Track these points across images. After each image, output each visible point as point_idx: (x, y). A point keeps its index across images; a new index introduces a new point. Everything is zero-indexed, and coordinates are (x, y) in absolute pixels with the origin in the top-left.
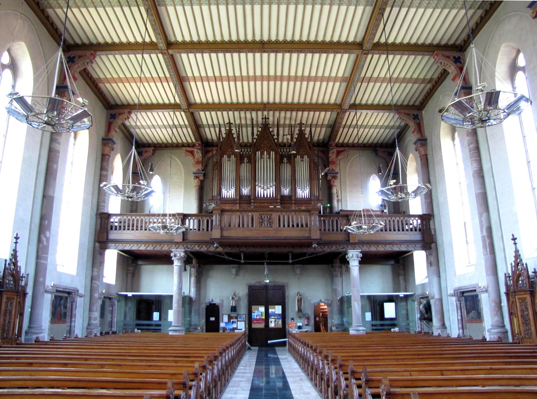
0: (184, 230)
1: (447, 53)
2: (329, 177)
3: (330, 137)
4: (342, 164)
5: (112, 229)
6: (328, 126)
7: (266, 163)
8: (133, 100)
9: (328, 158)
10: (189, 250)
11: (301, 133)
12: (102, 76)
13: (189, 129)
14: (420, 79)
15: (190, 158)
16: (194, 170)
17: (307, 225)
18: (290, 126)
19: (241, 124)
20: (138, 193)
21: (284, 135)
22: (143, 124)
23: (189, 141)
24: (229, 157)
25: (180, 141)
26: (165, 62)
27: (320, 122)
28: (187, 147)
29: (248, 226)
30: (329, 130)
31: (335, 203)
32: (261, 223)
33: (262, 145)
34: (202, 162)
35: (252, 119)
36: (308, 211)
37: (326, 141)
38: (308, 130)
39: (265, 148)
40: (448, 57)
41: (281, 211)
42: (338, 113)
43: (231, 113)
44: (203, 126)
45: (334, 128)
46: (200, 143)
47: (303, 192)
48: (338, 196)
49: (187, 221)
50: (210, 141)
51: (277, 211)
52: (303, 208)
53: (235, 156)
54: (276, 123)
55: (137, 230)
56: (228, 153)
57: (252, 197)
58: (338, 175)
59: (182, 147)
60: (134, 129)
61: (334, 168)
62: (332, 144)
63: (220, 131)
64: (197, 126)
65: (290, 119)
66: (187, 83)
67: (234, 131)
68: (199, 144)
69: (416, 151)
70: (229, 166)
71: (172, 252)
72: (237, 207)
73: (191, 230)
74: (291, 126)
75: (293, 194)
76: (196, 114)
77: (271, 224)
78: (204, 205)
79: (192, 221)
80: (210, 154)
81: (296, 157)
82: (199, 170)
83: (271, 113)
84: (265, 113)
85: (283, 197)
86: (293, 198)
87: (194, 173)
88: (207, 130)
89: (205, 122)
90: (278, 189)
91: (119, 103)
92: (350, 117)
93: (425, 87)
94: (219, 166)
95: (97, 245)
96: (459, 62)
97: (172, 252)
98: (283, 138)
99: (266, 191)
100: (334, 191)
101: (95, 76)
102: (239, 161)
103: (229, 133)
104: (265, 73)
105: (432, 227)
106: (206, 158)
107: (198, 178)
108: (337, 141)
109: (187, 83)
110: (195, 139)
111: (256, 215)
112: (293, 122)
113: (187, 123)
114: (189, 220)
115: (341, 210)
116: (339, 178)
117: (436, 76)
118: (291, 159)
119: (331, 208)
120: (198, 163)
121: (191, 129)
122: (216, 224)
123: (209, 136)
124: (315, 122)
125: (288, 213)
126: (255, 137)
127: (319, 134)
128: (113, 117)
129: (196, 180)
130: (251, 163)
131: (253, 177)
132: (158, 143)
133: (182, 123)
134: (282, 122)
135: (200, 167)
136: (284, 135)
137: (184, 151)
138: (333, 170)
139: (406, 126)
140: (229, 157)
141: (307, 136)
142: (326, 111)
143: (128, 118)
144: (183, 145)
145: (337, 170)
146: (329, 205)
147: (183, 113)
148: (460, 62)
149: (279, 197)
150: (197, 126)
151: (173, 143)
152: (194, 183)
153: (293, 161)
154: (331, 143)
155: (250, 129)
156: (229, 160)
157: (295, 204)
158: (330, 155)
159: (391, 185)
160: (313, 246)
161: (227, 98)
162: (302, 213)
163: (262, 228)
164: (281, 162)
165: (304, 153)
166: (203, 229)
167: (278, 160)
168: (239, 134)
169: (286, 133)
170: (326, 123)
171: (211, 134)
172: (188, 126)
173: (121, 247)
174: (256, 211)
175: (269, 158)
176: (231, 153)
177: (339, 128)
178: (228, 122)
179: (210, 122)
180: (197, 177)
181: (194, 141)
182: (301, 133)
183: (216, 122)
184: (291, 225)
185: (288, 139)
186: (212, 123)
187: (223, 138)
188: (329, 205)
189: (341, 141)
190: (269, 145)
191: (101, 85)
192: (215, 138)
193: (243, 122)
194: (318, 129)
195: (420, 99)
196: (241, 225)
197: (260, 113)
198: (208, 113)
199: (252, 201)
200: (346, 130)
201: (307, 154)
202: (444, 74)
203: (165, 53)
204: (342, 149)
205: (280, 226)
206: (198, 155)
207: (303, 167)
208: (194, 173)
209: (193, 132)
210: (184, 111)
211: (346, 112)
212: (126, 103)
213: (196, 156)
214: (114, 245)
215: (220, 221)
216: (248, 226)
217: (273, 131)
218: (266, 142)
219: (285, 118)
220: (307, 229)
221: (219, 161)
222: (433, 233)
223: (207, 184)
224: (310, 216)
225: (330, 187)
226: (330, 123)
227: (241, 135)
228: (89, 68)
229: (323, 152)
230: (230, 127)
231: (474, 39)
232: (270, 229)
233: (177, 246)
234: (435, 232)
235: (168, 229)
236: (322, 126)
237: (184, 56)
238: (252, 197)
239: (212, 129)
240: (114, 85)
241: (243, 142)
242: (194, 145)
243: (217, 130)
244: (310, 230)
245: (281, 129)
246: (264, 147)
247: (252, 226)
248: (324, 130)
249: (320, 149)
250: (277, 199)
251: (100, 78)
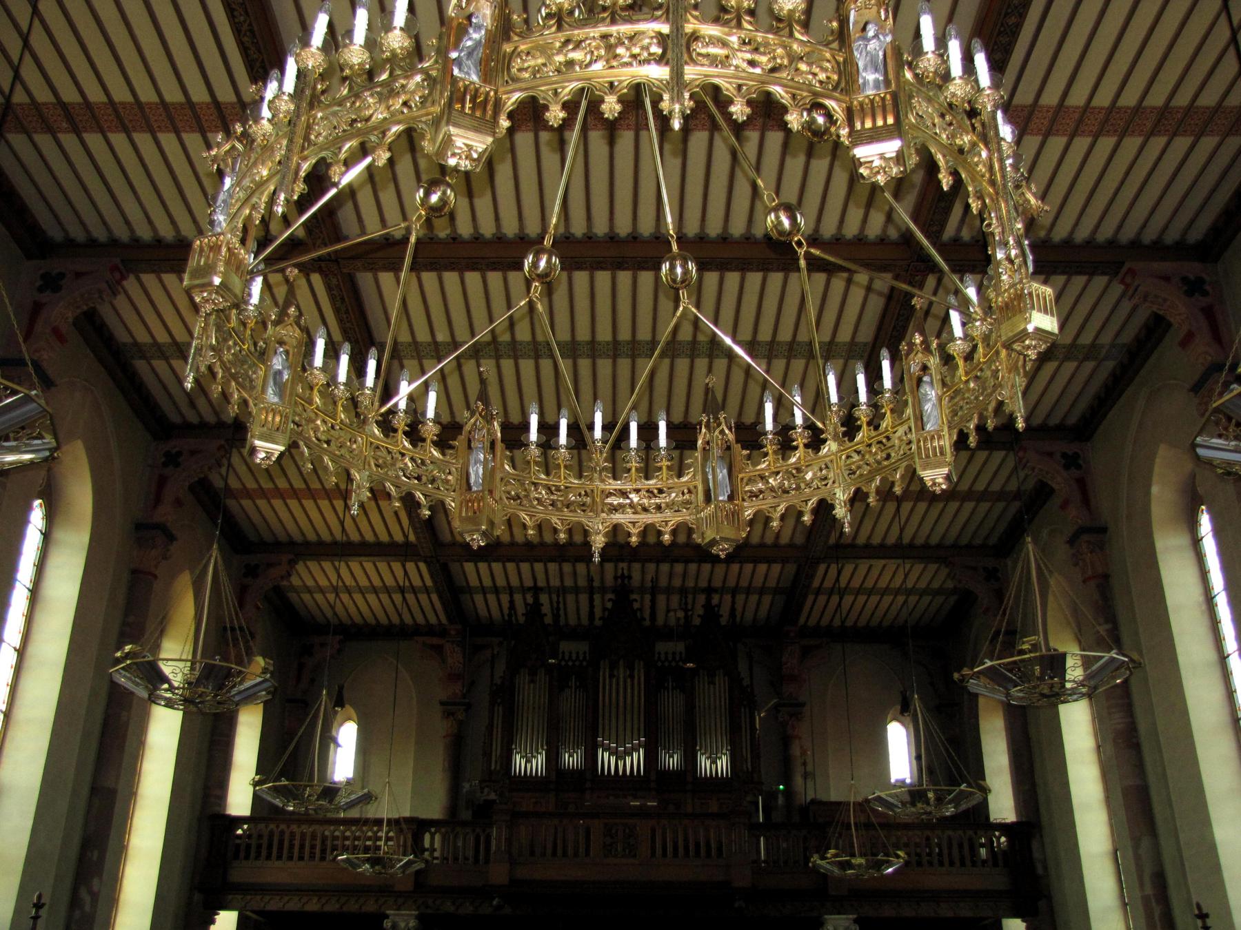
0: (419, 866)
1: (1166, 267)
5: (236, 857)
6: (776, 591)
8: (303, 534)
10: (429, 911)
11: (711, 612)
12: (142, 337)
13: (434, 597)
14: (1084, 347)
17: (720, 849)
18: (683, 591)
20: (221, 687)
21: (668, 611)
22: (321, 583)
29: (576, 855)
31: (798, 780)
40: (1050, 454)
43: (539, 567)
44: (469, 590)
45: (793, 595)
48: (805, 764)
49: (427, 837)
52: (714, 807)
55: (301, 858)
60: (298, 593)
63: (512, 602)
64: (452, 591)
67: (546, 609)
69: (1076, 565)
71: (387, 917)
76: (454, 567)
83: (637, 566)
85: (666, 774)
87: (442, 703)
88: (478, 598)
89: (474, 581)
91: (267, 537)
92: (826, 575)
93: (1005, 509)
95: (197, 897)
96: (995, 577)
97: (387, 917)
100: (796, 751)
101: (122, 336)
103: (534, 610)
104: (624, 335)
105: (1036, 855)
108: (802, 620)
110: (449, 618)
112: (690, 583)
113: (429, 583)
115: (813, 802)
117: (1127, 337)
121: (440, 598)
123: (482, 611)
127: (756, 608)
128: (252, 571)
132: (354, 624)
134: (663, 582)
136: (668, 611)
139: (1043, 492)
142: (770, 561)
143: (289, 575)
147: (422, 566)
148: (1079, 467)
149: (653, 776)
150: (452, 591)
151: (391, 625)
152: (441, 727)
155: (584, 598)
156: (532, 681)
159: (1022, 652)
160: (736, 905)
161: (510, 409)
166: (466, 859)
168: (558, 609)
170: (772, 583)
171: (487, 607)
173: (258, 902)
175: (632, 677)
181: (412, 538)
191: (140, 365)
194: (754, 598)
195: (1082, 406)
196: (560, 852)
200: (822, 599)
202: (1043, 492)
207: (713, 695)
208: (442, 703)
209: (443, 604)
211: (818, 563)
212: (282, 537)
214: (239, 897)
217: (640, 610)
219: (671, 575)
222: (1040, 871)
228: (105, 311)
230: (536, 599)
231: (1031, 521)
233: (400, 901)
234: (1045, 868)
235: (384, 867)
236: (762, 591)
239: (491, 598)
240: (262, 503)
243: (505, 599)
245: (661, 599)
248: (767, 599)
251: (136, 344)
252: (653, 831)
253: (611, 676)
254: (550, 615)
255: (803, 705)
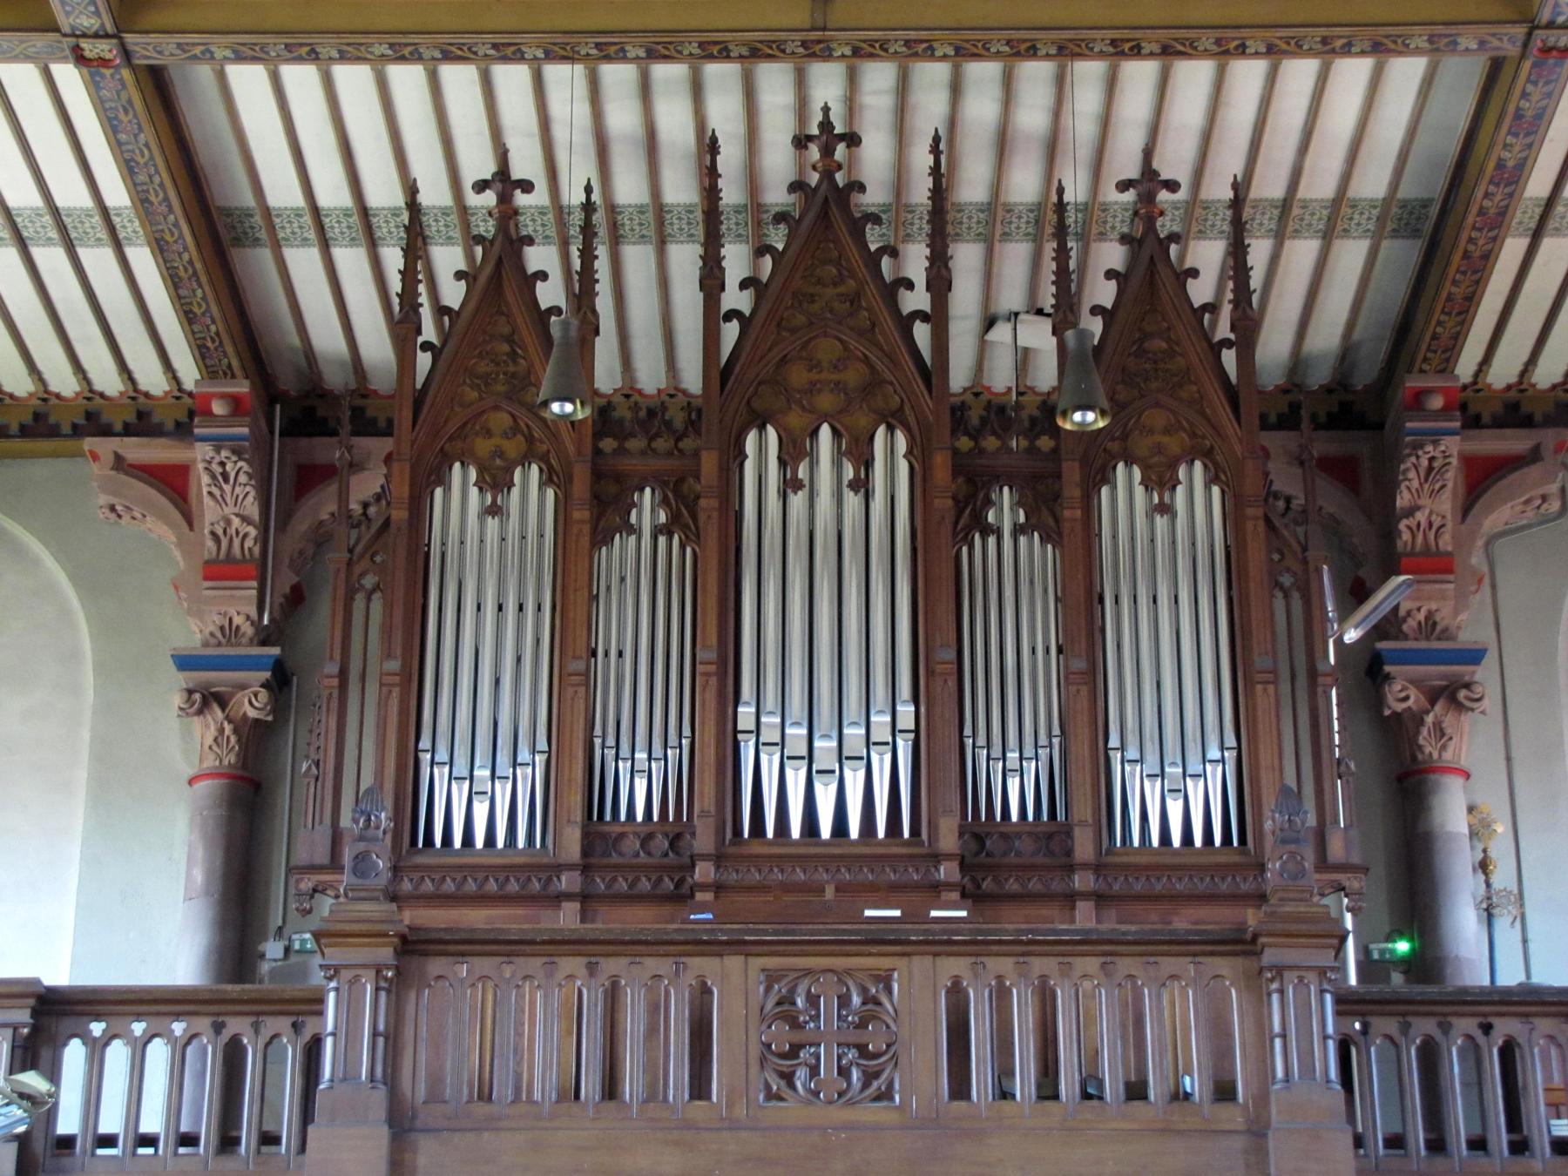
2: (1401, 694)
3: (1404, 329)
4: (1515, 581)
6: (1397, 217)
7: (828, 514)
9: (1385, 519)
11: (1152, 267)
15: (157, 528)
16: (192, 634)
18: (1057, 224)
19: (612, 209)
23: (152, 379)
24: (496, 481)
25: (63, 382)
26: (112, 128)
27: (1320, 185)
28: (128, 431)
29: (654, 1093)
30: (1402, 255)
31: (1464, 926)
32: (785, 1060)
33: (798, 376)
34: (259, 570)
35: (709, 146)
36: (1241, 944)
37: (1366, 373)
38: (1207, 255)
39: (826, 401)
41: (976, 946)
42: (1496, 67)
46: (242, 387)
47: (1175, 794)
48: (1484, 866)
49: (74, 1055)
50: (336, 379)
51: (941, 943)
53: (548, 479)
54: (920, 191)
56: (483, 446)
57: (703, 841)
58: (1485, 675)
59: (77, 432)
61: (1444, 617)
62: (1419, 396)
64: (209, 229)
65: (1052, 148)
66: (265, 255)
67: (539, 257)
68: (236, 402)
70: (489, 532)
72: (567, 917)
73: (108, 1141)
74: (1061, 231)
75: (1083, 810)
77: (872, 1064)
78: (273, 949)
79: (117, 1056)
80: (322, 504)
81: (1104, 476)
82: (230, 633)
83: (879, 77)
84: (827, 84)
86: (1084, 848)
87: (185, 662)
88: (304, 263)
90: (940, 751)
94: (404, 563)
98: (983, 346)
99: (830, 765)
100: (1452, 811)
102: (581, 514)
106: (302, 524)
107: (222, 701)
108: (1465, 368)
109: (265, 255)
110: (202, 352)
111: (736, 986)
113: (117, 195)
114: (96, 1052)
116: (1491, 703)
118: (1059, 491)
119: (1428, 964)
120: (219, 570)
121: (160, 248)
122: (346, 1075)
123: (326, 336)
124: (1269, 185)
125: (1039, 965)
126: (735, 298)
129: (206, 729)
130: (692, 536)
131: (708, 654)
133: (71, 193)
134: (972, 187)
135: (241, 605)
136: (990, 323)
137: (100, 470)
138: (1430, 627)
140: (496, 481)
141: (1200, 292)
144: (92, 419)
145: (1471, 628)
146: (1403, 947)
147: (68, 75)
152: (183, 752)
153: (1071, 514)
154: (1413, 382)
155: (685, 258)
156: (494, 510)
157: (1101, 899)
158: (1403, 500)
162: (1168, 964)
163: (791, 1110)
164: (970, 518)
165: (1173, 444)
167: (943, 504)
169: (1011, 296)
170: (1373, 183)
171: (338, 308)
172: (130, 225)
174: (737, 946)
175: (862, 485)
176: (513, 447)
177: (1497, 224)
178: (488, 170)
179: (332, 192)
180: (207, 699)
181: (189, 372)
182: (1152, 267)
183: (383, 192)
184: (1068, 1084)
185: (1024, 358)
186: (345, 199)
187: (441, 311)
188: (1403, 947)
189: (1503, 373)
190: (853, 376)
192: (376, 345)
193: (629, 189)
194: (1302, 253)
196: (590, 1086)
197: (775, 81)
198: (301, 78)
199: (704, 872)
201: (1207, 455)
203: (104, 62)
204: (1513, 442)
205: (960, 1089)
206: (229, 500)
208: (185, 662)
209: (174, 281)
210: (80, 59)
213: (210, 513)
215: (391, 1040)
216: (654, 1093)
218: (827, 350)
220: (1232, 1117)
221: (399, 515)
223: (296, 765)
224: (1256, 987)
225: (1407, 785)
226: (1405, 192)
227: (604, 288)
229: (1343, 471)
232: (872, 1113)
236: (1336, 217)
237: (248, 81)
238: (703, 841)
239: (351, 261)
241: (630, 391)
242: (181, 418)
243: (393, 259)
244: (1258, 1132)
245: (966, 258)
246: (812, 389)
247: (699, 1089)
248: (1351, 255)
249: (1325, 444)
250: (936, 858)
252: (957, 996)
253: (790, 485)
254: (556, 274)
255: (1474, 656)
